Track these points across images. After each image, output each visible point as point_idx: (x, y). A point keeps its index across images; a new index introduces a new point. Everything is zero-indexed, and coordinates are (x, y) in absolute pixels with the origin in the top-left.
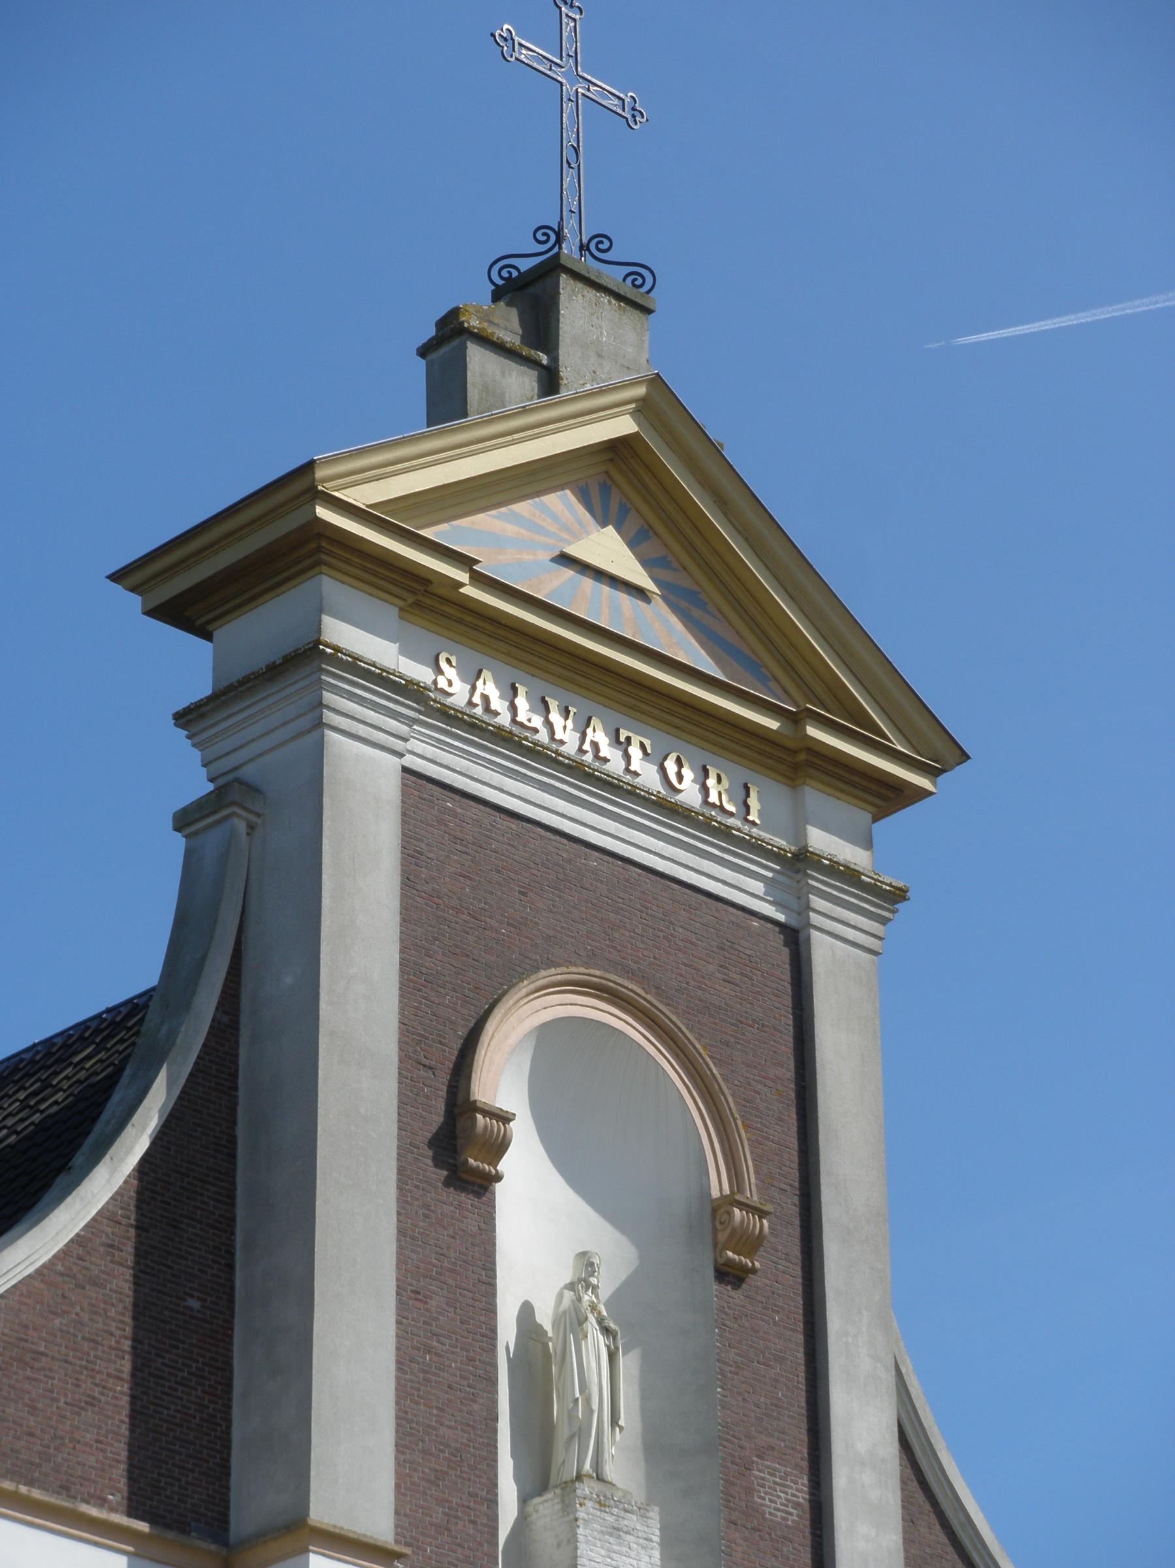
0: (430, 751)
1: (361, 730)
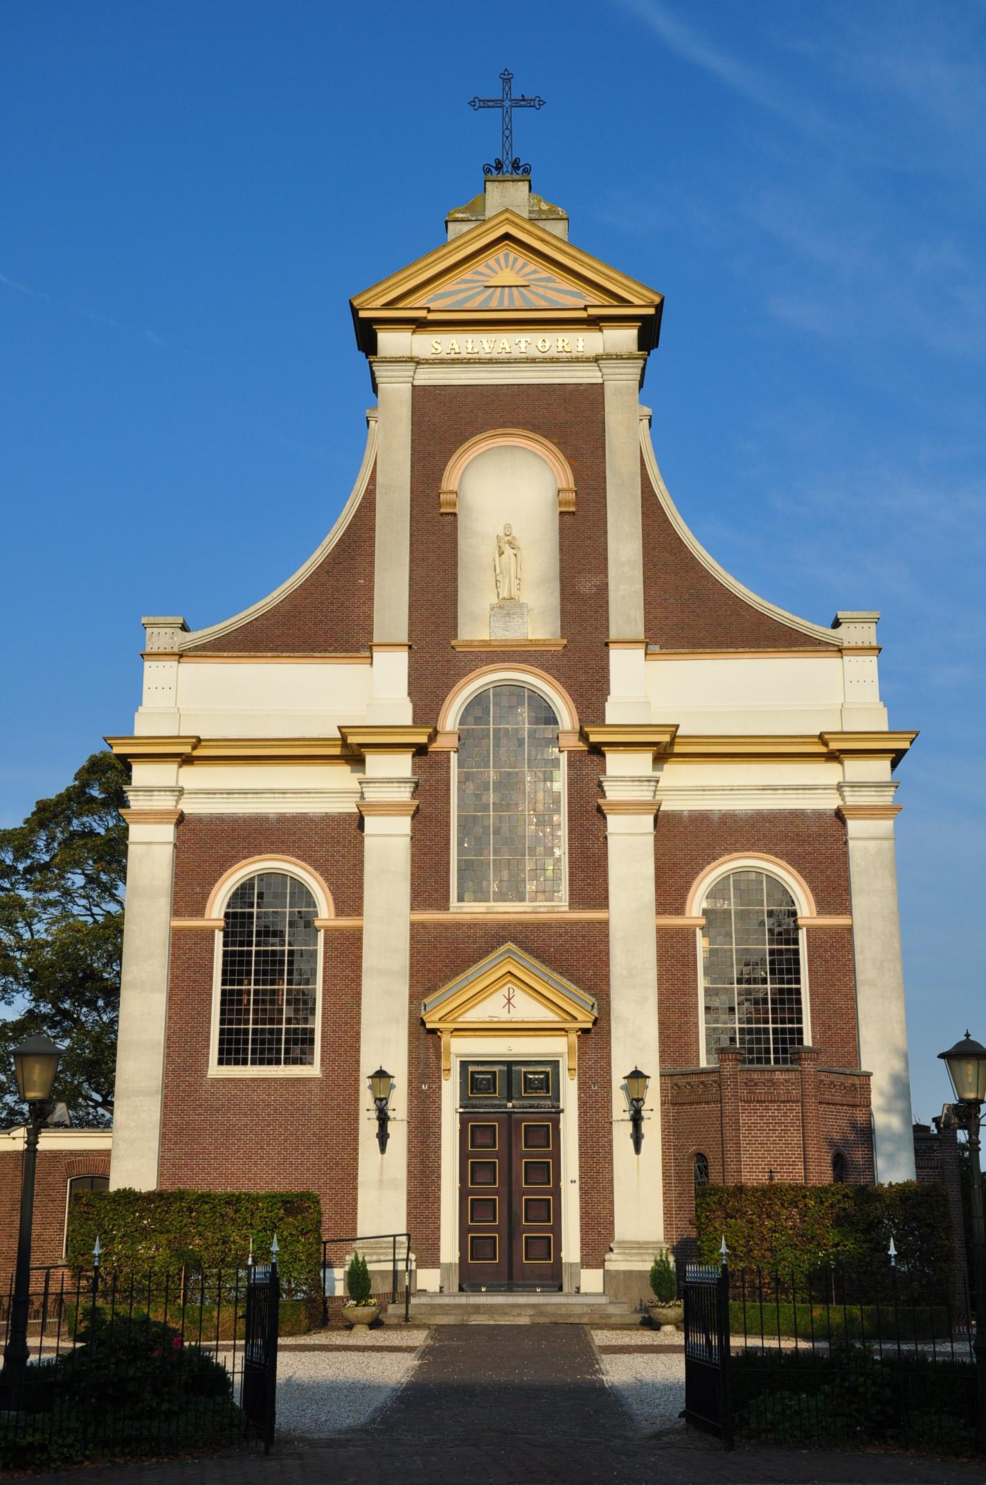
1: (393, 380)
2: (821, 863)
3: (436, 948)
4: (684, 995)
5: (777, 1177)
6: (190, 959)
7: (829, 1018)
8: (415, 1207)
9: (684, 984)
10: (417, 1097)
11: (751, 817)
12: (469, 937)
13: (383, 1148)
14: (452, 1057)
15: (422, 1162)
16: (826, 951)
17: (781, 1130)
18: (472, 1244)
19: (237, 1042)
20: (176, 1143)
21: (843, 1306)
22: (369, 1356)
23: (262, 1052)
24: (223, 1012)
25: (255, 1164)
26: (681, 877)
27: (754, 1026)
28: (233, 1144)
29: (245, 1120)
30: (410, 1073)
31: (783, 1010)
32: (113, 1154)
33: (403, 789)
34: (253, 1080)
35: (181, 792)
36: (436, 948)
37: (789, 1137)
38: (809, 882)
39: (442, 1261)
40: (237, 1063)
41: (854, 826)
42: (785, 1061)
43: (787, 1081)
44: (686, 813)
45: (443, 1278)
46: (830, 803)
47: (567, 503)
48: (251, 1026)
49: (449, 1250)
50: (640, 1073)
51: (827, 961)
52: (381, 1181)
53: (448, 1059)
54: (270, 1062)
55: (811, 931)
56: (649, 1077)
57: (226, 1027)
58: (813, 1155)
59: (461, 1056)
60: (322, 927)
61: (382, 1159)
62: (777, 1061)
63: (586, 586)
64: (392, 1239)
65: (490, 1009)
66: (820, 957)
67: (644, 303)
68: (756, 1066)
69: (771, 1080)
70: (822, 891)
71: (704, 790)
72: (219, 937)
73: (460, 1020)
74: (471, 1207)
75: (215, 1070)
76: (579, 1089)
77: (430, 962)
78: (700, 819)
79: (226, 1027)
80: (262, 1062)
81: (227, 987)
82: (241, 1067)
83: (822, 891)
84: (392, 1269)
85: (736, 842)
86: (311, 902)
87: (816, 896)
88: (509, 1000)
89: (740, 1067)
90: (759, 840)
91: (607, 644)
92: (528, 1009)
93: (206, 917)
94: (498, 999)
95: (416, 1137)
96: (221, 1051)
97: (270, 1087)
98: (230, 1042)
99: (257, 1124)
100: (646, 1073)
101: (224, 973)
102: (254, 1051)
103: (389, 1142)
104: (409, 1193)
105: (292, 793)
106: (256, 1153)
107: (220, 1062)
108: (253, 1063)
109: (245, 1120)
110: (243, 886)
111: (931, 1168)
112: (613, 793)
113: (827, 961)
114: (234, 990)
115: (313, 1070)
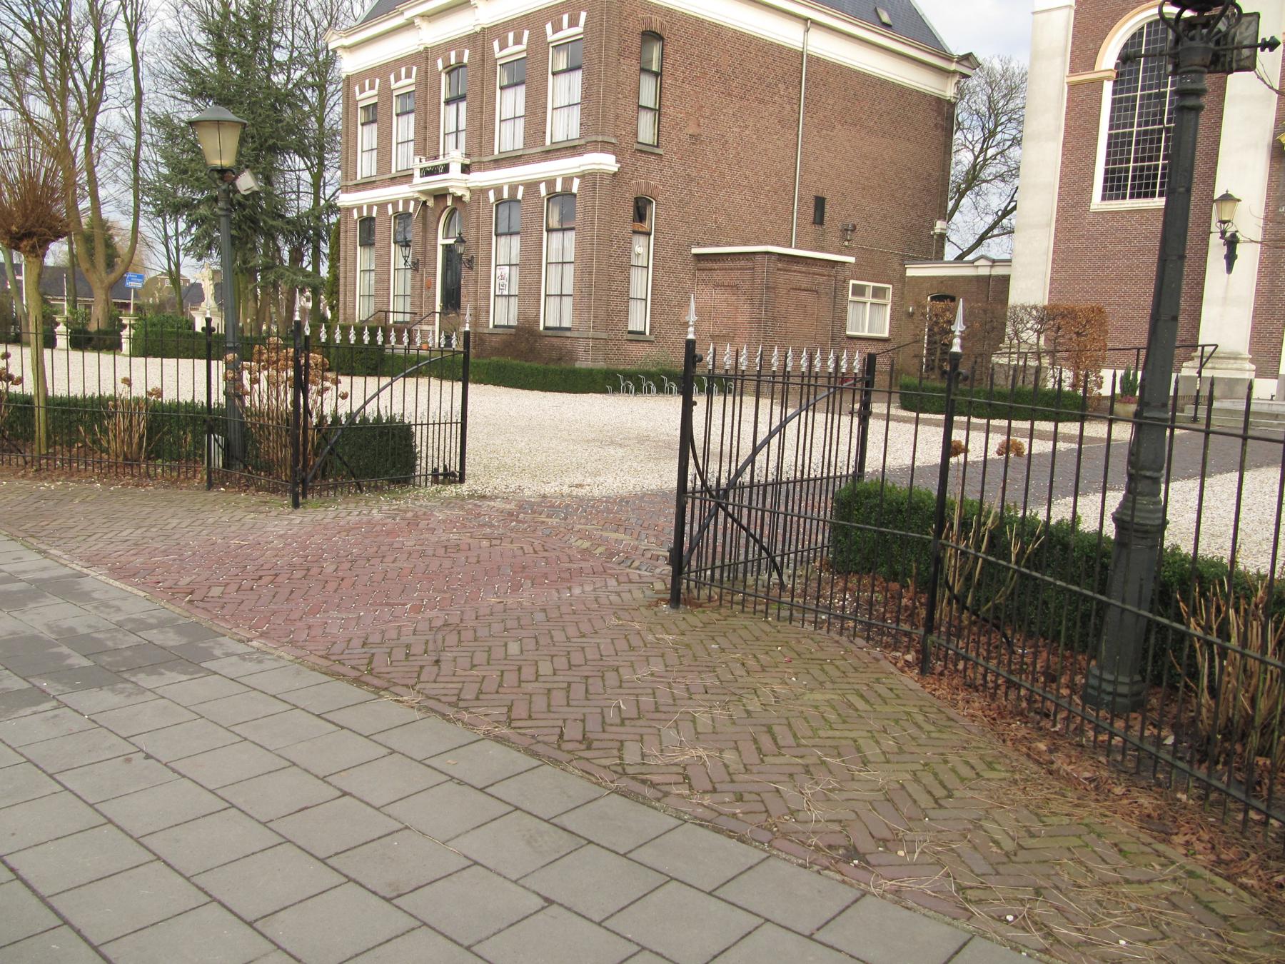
6: (1081, 110)
13: (1229, 268)
15: (1272, 281)
19: (1119, 179)
20: (1062, 267)
21: (515, 291)
24: (1108, 154)
25: (1126, 284)
28: (1109, 267)
30: (1268, 197)
34: (1129, 212)
35: (457, 131)
39: (1281, 372)
40: (1117, 198)
50: (1230, 196)
54: (1146, 196)
56: (1239, 200)
72: (1108, 87)
75: (1097, 202)
80: (1139, 196)
81: (1113, 132)
82: (1120, 201)
93: (1096, 69)
95: (1268, 257)
96: (1105, 189)
97: (1142, 217)
98: (1112, 180)
99: (1129, 250)
100: (1236, 196)
101: (1112, 119)
102: (1133, 187)
104: (1255, 310)
106: (1127, 275)
107: (1104, 198)
108: (1132, 197)
110: (1133, 36)
115: (1097, 202)
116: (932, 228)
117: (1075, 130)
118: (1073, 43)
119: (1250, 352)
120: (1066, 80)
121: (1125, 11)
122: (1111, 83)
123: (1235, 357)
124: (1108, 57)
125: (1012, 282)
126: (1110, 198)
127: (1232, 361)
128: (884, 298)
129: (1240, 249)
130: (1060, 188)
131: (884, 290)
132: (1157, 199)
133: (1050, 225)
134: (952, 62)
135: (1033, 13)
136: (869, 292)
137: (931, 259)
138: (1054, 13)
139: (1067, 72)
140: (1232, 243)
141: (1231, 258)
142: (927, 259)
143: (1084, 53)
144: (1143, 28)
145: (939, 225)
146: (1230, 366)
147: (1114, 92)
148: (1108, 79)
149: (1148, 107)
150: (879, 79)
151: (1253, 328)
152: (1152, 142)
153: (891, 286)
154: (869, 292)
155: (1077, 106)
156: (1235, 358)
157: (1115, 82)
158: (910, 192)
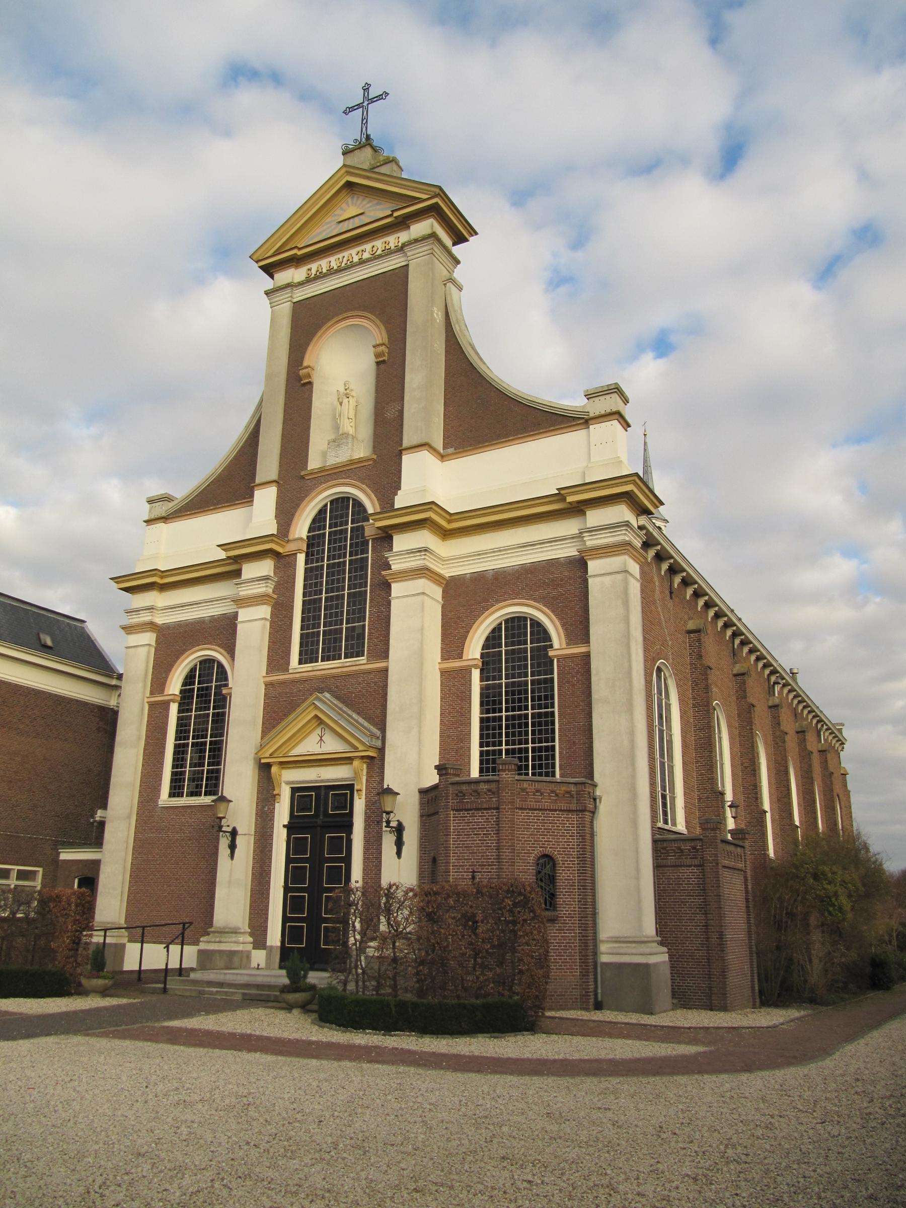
0: (303, 293)
2: (571, 601)
3: (279, 702)
4: (461, 725)
5: (478, 876)
7: (574, 735)
8: (255, 902)
9: (462, 715)
10: (261, 817)
11: (517, 571)
12: (300, 691)
13: (399, 854)
14: (283, 785)
16: (573, 677)
17: (484, 834)
18: (290, 933)
22: (7, 1006)
23: (540, 766)
26: (463, 627)
27: (517, 746)
29: (177, 836)
31: (540, 732)
32: (102, 862)
33: (261, 585)
36: (279, 702)
37: (490, 840)
38: (561, 619)
39: (268, 944)
41: (593, 566)
42: (540, 774)
43: (489, 790)
44: (468, 576)
45: (269, 957)
46: (569, 551)
47: (382, 354)
48: (530, 745)
49: (274, 936)
51: (573, 685)
52: (230, 882)
53: (280, 785)
55: (561, 658)
56: (231, 801)
57: (537, 745)
58: (506, 856)
59: (293, 783)
60: (555, 656)
61: (399, 862)
62: (533, 774)
63: (390, 414)
64: (181, 926)
65: (310, 746)
66: (568, 682)
67: (427, 197)
68: (544, 778)
69: (476, 791)
70: (571, 625)
71: (479, 555)
72: (476, 674)
73: (294, 752)
74: (292, 904)
76: (366, 806)
77: (275, 712)
78: (479, 578)
79: (537, 745)
83: (571, 625)
84: (184, 946)
85: (505, 593)
86: (547, 637)
87: (566, 629)
88: (321, 737)
89: (517, 777)
90: (523, 589)
91: (253, 487)
92: (332, 745)
93: (464, 658)
94: (314, 737)
100: (396, 790)
103: (237, 851)
105: (540, 544)
108: (206, 794)
109: (177, 836)
110: (494, 631)
111: (695, 866)
112: (397, 565)
113: (573, 685)
114: (496, 716)
116: (93, 816)
117: (152, 740)
118: (153, 672)
119: (250, 926)
120: (146, 700)
121: (185, 651)
122: (478, 671)
123: (235, 932)
124: (474, 649)
125: (102, 867)
126: (174, 796)
127: (234, 935)
128: (34, 880)
129: (239, 840)
130: (140, 786)
131: (35, 872)
132: (203, 797)
133: (129, 817)
134: (113, 678)
135: (127, 648)
136: (14, 875)
137: (90, 844)
138: (140, 649)
139: (148, 694)
140: (399, 830)
141: (399, 844)
142: (85, 844)
143: (159, 682)
144: (196, 665)
145: (100, 813)
146: (230, 940)
147: (179, 712)
148: (476, 666)
149: (513, 694)
150: (33, 690)
151: (251, 906)
152: (520, 726)
153: (40, 869)
154: (14, 875)
155: (153, 721)
156: (236, 933)
157: (482, 670)
158: (66, 785)
